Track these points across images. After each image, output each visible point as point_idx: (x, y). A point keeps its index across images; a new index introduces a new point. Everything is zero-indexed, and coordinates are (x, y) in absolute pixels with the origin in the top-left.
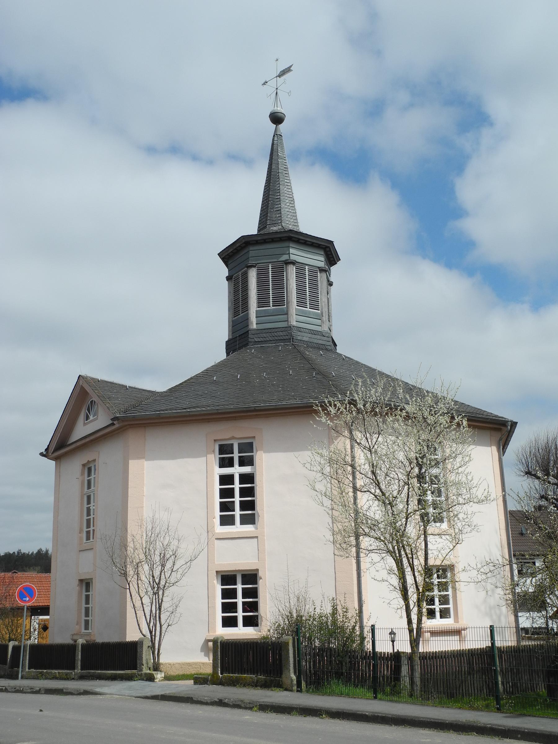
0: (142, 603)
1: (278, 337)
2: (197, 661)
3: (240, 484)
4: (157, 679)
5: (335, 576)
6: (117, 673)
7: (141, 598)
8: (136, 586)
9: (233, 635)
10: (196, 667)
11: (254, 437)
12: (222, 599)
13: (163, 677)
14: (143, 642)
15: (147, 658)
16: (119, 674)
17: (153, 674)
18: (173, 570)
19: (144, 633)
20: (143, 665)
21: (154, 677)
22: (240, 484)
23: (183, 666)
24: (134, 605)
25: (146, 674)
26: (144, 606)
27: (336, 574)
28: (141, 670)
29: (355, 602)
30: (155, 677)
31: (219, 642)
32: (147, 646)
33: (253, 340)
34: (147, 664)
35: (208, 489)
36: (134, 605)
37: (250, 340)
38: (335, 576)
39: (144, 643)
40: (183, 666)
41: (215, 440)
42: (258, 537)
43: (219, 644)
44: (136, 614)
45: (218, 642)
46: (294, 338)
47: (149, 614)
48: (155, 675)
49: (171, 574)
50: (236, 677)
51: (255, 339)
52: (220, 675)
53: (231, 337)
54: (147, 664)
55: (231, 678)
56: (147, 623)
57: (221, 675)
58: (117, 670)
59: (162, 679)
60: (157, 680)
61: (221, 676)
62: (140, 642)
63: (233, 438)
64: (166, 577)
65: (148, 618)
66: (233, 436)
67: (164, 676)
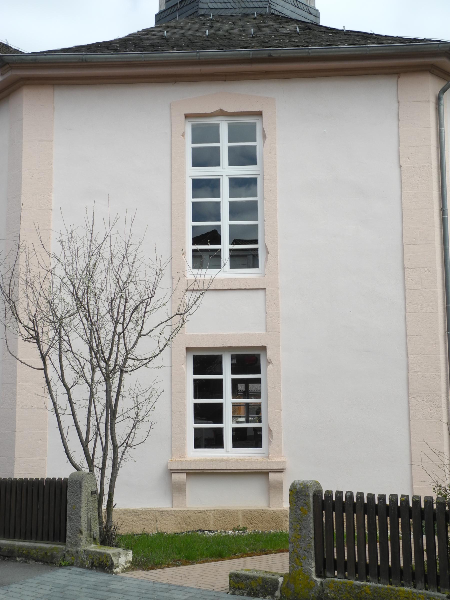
0: (70, 400)
1: (247, 4)
2: (148, 507)
3: (230, 197)
4: (118, 567)
5: (408, 362)
6: (14, 546)
7: (68, 390)
8: (57, 364)
9: (212, 461)
10: (149, 518)
11: (259, 114)
12: (195, 397)
13: (129, 562)
14: (80, 483)
15: (89, 516)
16: (20, 547)
17: (108, 556)
18: (142, 333)
19: (77, 460)
20: (81, 532)
21: (112, 564)
22: (230, 197)
23: (122, 516)
24: (54, 404)
25: (88, 553)
26: (75, 406)
27: (409, 359)
28: (77, 544)
29: (443, 409)
30: (115, 562)
31: (311, 495)
32: (90, 491)
33: (205, 6)
34: (90, 529)
35: (173, 202)
36: (54, 404)
37: (201, 5)
38: (408, 362)
39: (83, 485)
40: (122, 516)
41: (187, 116)
42: (265, 289)
43: (311, 499)
44: (59, 422)
45: (308, 496)
46: (272, 6)
47: (86, 423)
48: (113, 559)
49: (136, 342)
50: (375, 590)
51: (210, 4)
52: (315, 578)
53: (164, 8)
54: (90, 529)
55: (357, 591)
56: (81, 440)
57: (318, 576)
58: (14, 537)
59: (129, 565)
60: (117, 569)
61: (319, 580)
62: (75, 482)
63: (221, 113)
64: (127, 346)
65: (83, 430)
66: (221, 110)
67: (131, 560)
